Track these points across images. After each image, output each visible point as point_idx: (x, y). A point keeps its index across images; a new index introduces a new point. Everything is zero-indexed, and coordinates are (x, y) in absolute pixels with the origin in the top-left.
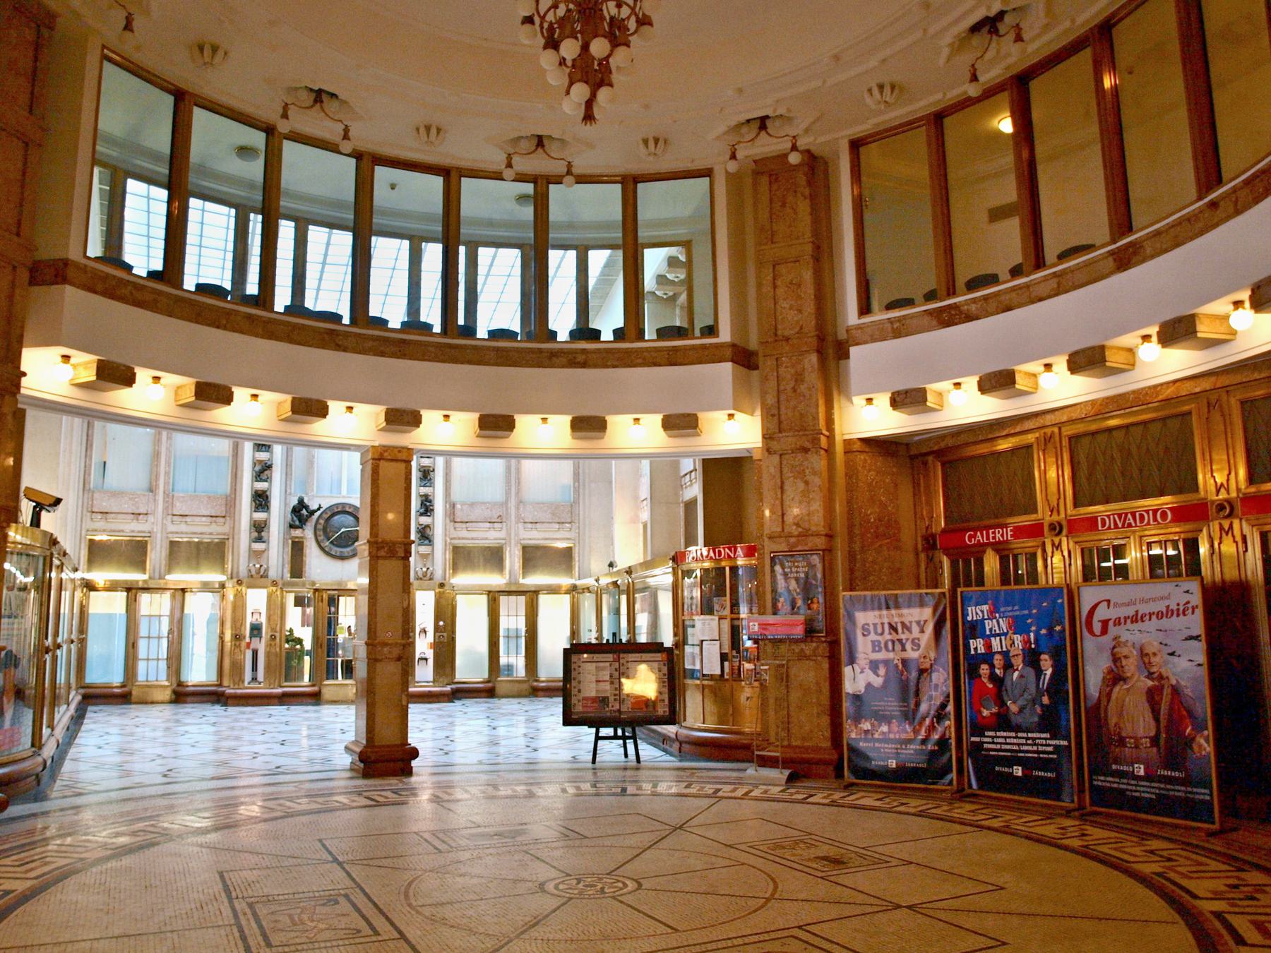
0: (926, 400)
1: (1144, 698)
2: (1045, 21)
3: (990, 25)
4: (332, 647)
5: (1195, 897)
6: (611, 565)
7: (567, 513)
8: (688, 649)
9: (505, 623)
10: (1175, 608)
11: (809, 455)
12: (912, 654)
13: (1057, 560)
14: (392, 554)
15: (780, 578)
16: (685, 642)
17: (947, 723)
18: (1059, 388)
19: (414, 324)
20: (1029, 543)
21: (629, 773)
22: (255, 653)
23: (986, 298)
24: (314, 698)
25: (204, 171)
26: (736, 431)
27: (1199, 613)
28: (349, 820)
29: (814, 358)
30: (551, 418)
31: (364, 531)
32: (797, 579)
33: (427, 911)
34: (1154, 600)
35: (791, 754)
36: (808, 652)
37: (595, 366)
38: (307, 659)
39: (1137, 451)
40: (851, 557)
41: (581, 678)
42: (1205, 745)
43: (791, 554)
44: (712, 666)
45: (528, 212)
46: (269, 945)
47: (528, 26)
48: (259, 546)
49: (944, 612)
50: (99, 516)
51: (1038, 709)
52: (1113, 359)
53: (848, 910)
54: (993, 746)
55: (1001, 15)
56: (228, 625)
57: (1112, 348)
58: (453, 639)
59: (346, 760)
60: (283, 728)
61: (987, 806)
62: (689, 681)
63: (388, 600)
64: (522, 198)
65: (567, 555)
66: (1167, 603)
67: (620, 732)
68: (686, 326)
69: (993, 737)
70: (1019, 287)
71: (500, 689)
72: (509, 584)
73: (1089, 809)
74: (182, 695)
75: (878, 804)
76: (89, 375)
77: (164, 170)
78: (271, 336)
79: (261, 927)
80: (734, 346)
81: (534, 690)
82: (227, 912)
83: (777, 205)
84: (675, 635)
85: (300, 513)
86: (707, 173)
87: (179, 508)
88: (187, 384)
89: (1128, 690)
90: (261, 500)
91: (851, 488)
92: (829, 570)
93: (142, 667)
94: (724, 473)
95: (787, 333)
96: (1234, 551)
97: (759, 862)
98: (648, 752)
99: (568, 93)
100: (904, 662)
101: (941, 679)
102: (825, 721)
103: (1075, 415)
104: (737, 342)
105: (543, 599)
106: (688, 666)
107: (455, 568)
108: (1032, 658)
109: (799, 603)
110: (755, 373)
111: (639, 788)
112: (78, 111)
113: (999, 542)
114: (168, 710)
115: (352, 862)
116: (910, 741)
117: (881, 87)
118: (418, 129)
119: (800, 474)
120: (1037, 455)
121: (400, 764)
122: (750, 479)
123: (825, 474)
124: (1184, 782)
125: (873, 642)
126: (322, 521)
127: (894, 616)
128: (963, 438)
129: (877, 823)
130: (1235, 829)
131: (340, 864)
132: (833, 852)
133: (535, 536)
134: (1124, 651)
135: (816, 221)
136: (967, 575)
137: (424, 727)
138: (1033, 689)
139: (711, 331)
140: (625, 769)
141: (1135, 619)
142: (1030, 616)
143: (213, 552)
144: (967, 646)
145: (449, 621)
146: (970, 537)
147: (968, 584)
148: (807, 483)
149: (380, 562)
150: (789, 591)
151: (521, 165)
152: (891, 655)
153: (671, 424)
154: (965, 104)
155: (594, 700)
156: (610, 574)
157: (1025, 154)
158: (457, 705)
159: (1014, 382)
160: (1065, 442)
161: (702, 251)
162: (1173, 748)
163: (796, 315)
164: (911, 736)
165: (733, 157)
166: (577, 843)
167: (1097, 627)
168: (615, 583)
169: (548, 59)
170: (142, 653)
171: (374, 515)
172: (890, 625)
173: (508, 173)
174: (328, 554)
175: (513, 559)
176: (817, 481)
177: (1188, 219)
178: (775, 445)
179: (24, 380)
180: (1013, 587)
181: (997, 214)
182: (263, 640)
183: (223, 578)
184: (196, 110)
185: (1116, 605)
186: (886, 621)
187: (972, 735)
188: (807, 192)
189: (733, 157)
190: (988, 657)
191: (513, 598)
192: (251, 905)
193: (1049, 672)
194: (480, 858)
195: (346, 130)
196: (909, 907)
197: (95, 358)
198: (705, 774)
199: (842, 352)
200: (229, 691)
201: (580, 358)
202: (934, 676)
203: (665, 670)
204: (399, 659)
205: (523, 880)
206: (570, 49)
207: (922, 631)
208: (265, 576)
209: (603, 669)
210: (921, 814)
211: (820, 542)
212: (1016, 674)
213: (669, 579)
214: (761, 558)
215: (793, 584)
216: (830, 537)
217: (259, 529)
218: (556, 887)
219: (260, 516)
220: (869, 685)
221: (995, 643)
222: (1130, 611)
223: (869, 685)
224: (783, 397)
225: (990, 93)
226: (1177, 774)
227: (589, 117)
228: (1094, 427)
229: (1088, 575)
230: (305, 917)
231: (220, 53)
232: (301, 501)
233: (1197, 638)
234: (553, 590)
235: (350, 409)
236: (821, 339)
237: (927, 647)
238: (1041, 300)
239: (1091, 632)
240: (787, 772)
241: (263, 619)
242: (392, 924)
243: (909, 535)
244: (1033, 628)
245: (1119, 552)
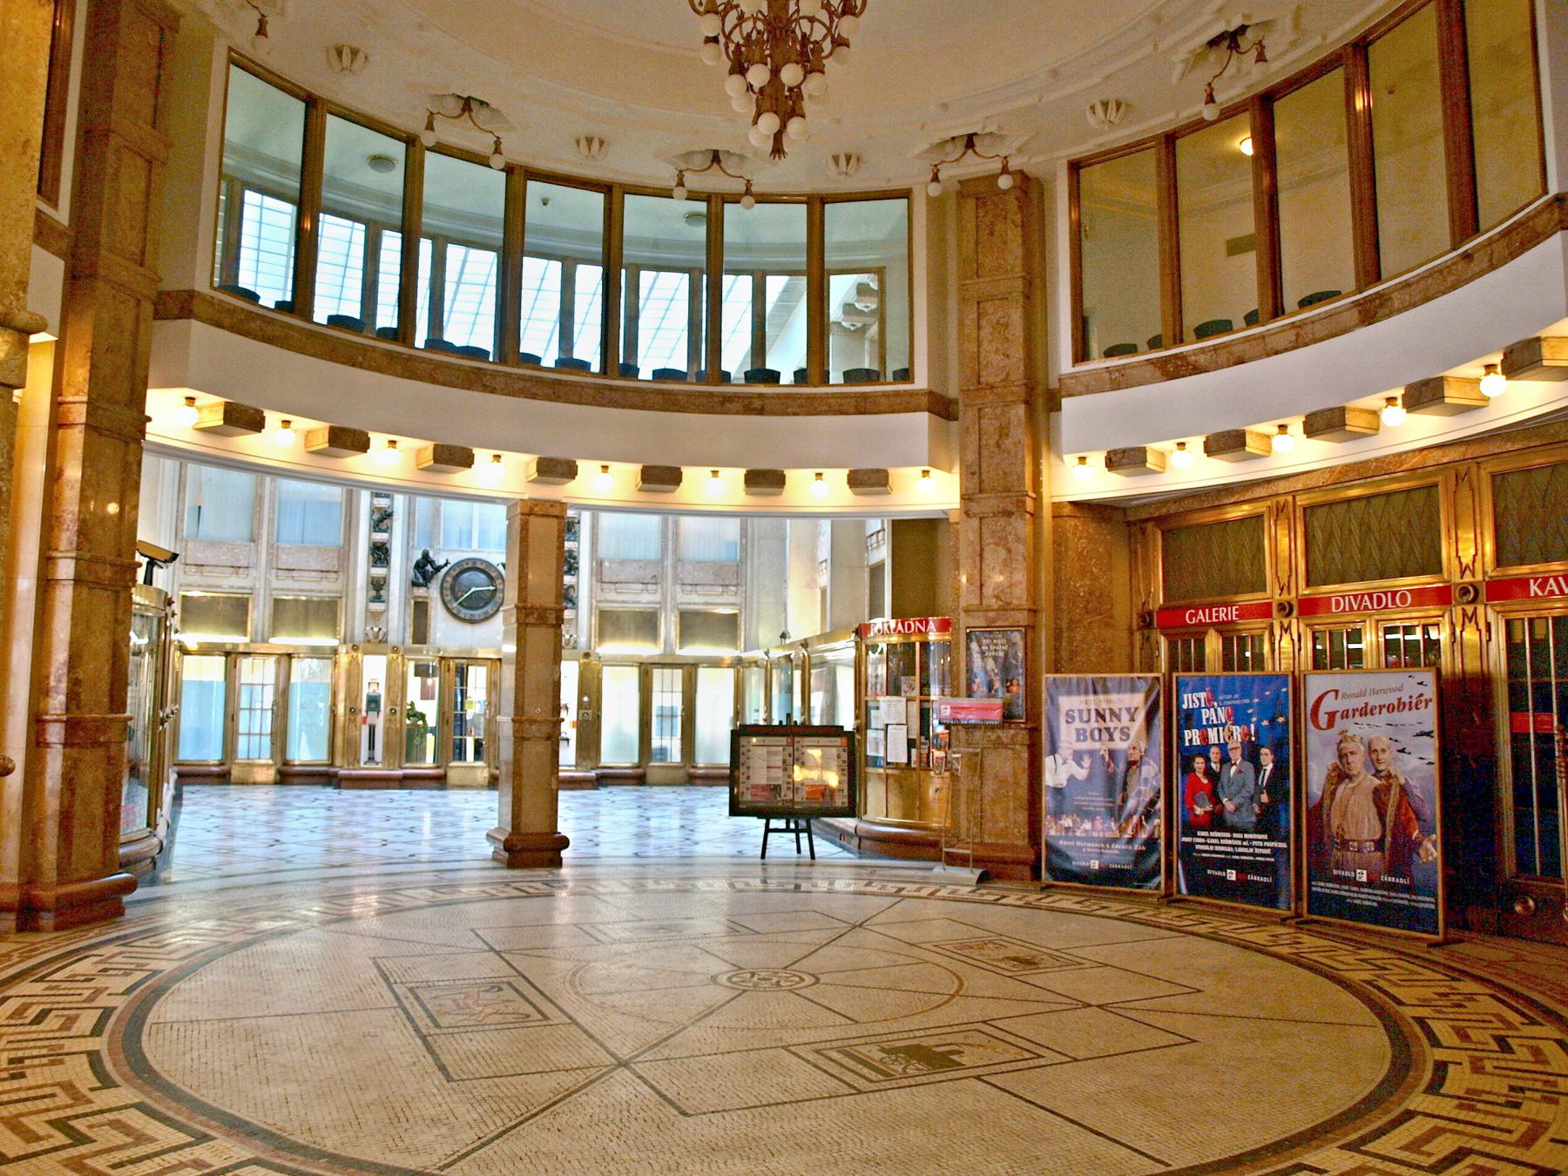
0: (1145, 461)
1: (1370, 796)
2: (1292, 38)
3: (1230, 40)
4: (461, 723)
5: (1400, 1003)
6: (783, 636)
7: (731, 573)
8: (871, 734)
9: (658, 701)
10: (1407, 700)
11: (1013, 519)
12: (1120, 745)
13: (1286, 643)
14: (542, 620)
15: (976, 657)
16: (867, 725)
17: (1157, 821)
18: (1295, 453)
19: (568, 363)
20: (1256, 624)
21: (803, 869)
22: (372, 729)
23: (1216, 348)
24: (439, 781)
25: (337, 184)
26: (931, 490)
27: (1433, 706)
28: (487, 913)
29: (1021, 410)
30: (723, 471)
31: (511, 594)
32: (995, 659)
33: (596, 1000)
34: (1385, 691)
35: (982, 853)
36: (1005, 740)
37: (773, 413)
38: (430, 739)
39: (1374, 526)
40: (1057, 636)
41: (751, 763)
42: (1431, 851)
43: (989, 630)
44: (899, 754)
45: (700, 232)
46: (438, 1026)
47: (711, 45)
48: (376, 607)
49: (1156, 702)
50: (194, 569)
51: (1257, 809)
52: (1354, 422)
53: (1034, 1008)
55: (1242, 29)
56: (341, 696)
57: (1354, 410)
58: (599, 717)
59: (488, 849)
60: (408, 813)
61: (1195, 912)
62: (871, 770)
63: (536, 672)
64: (692, 217)
65: (732, 621)
66: (1399, 695)
67: (792, 826)
68: (875, 367)
71: (652, 775)
72: (664, 655)
73: (1306, 916)
74: (287, 776)
75: (1077, 907)
76: (217, 419)
77: (295, 183)
78: (413, 375)
79: (426, 1010)
80: (930, 393)
81: (692, 777)
82: (388, 995)
83: (984, 234)
84: (857, 717)
85: (424, 569)
86: (906, 194)
87: (286, 560)
88: (320, 428)
89: (1353, 789)
90: (380, 553)
91: (1058, 556)
92: (1030, 648)
93: (242, 743)
94: (917, 537)
95: (991, 380)
96: (1478, 642)
97: (944, 961)
98: (823, 847)
99: (755, 122)
100: (1112, 753)
101: (1151, 774)
102: (1022, 817)
103: (1312, 483)
104: (938, 391)
105: (703, 673)
106: (870, 753)
107: (602, 635)
108: (1252, 753)
109: (997, 685)
110: (954, 424)
111: (815, 886)
112: (202, 120)
113: (1223, 623)
114: (273, 793)
115: (510, 952)
116: (1114, 840)
117: (1105, 105)
118: (578, 142)
119: (1002, 541)
120: (1267, 524)
121: (549, 855)
122: (944, 541)
123: (1030, 541)
124: (1408, 889)
126: (449, 579)
127: (1101, 702)
128: (1186, 505)
129: (1075, 925)
130: (1461, 941)
131: (498, 953)
132: (1023, 953)
133: (695, 600)
134: (1349, 746)
135: (1028, 256)
136: (1188, 659)
137: (571, 814)
138: (1251, 786)
139: (905, 375)
140: (798, 865)
141: (1365, 711)
142: (1250, 706)
143: (324, 612)
144: (1181, 738)
145: (594, 697)
146: (1191, 616)
147: (1188, 669)
148: (1009, 551)
149: (529, 629)
150: (986, 672)
151: (693, 182)
152: (1097, 745)
153: (855, 480)
154: (1199, 125)
155: (764, 788)
156: (783, 647)
157: (1266, 181)
158: (603, 794)
159: (1244, 445)
160: (1299, 513)
161: (897, 280)
162: (1399, 852)
163: (1005, 361)
164: (1117, 834)
165: (935, 178)
166: (749, 938)
167: (1323, 719)
168: (788, 657)
169: (734, 84)
170: (243, 727)
171: (523, 577)
172: (1097, 712)
173: (678, 192)
174: (456, 616)
175: (669, 626)
176: (1020, 549)
177: (1439, 271)
178: (975, 508)
179: (148, 425)
180: (1236, 673)
181: (1235, 247)
182: (382, 714)
183: (334, 642)
184: (329, 117)
186: (1093, 707)
187: (1185, 835)
188: (1018, 218)
189: (935, 178)
190: (1203, 751)
191: (667, 671)
192: (411, 990)
193: (1269, 767)
194: (646, 950)
195: (498, 143)
196: (1100, 1006)
197: (222, 400)
198: (886, 872)
199: (1053, 404)
200: (342, 772)
201: (757, 404)
202: (1145, 769)
203: (845, 756)
204: (548, 738)
205: (694, 973)
206: (758, 75)
207: (1133, 720)
208: (384, 641)
209: (776, 753)
210: (1121, 918)
211: (1022, 618)
212: (1234, 769)
213: (850, 654)
214: (956, 634)
215: (991, 664)
216: (1034, 612)
217: (378, 587)
218: (729, 979)
219: (379, 572)
220: (1071, 778)
222: (1359, 703)
223: (1071, 778)
224: (985, 453)
225: (1230, 113)
226: (1402, 881)
227: (778, 150)
228: (1330, 497)
229: (1318, 664)
230: (470, 1002)
231: (361, 57)
232: (426, 556)
233: (1429, 734)
234: (715, 663)
235: (498, 457)
236: (1030, 389)
237: (1137, 738)
238: (1277, 353)
239: (1318, 727)
240: (978, 872)
241: (382, 691)
242: (561, 1010)
243: (1124, 612)
245: (1356, 636)
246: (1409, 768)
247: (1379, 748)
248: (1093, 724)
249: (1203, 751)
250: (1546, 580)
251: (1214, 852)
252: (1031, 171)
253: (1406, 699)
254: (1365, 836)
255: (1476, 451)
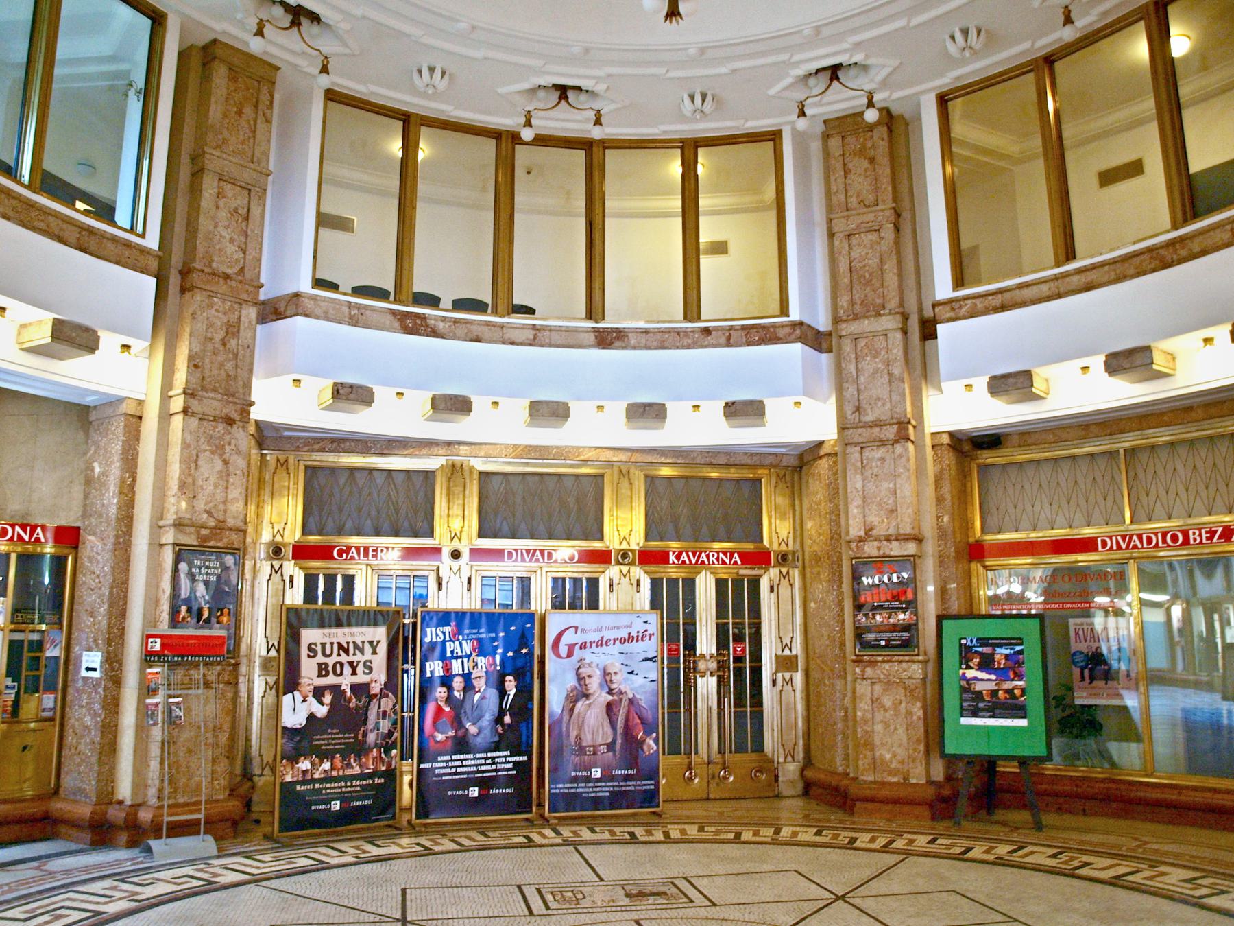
32: (206, 583)
54: (448, 771)
69: (447, 762)
70: (493, 325)
125: (320, 665)
141: (600, 643)
148: (226, 462)
167: (563, 650)
178: (195, 405)
181: (720, 248)
185: (582, 631)
193: (512, 692)
199: (929, 332)
207: (374, 653)
212: (477, 696)
215: (201, 589)
220: (311, 717)
221: (456, 666)
222: (596, 637)
223: (311, 717)
238: (512, 343)
239: (559, 656)
244: (500, 651)
246: (636, 685)
247: (612, 671)
248: (334, 659)
249: (446, 681)
250: (680, 554)
251: (456, 774)
252: (895, 110)
253: (634, 634)
254: (600, 741)
255: (638, 457)
